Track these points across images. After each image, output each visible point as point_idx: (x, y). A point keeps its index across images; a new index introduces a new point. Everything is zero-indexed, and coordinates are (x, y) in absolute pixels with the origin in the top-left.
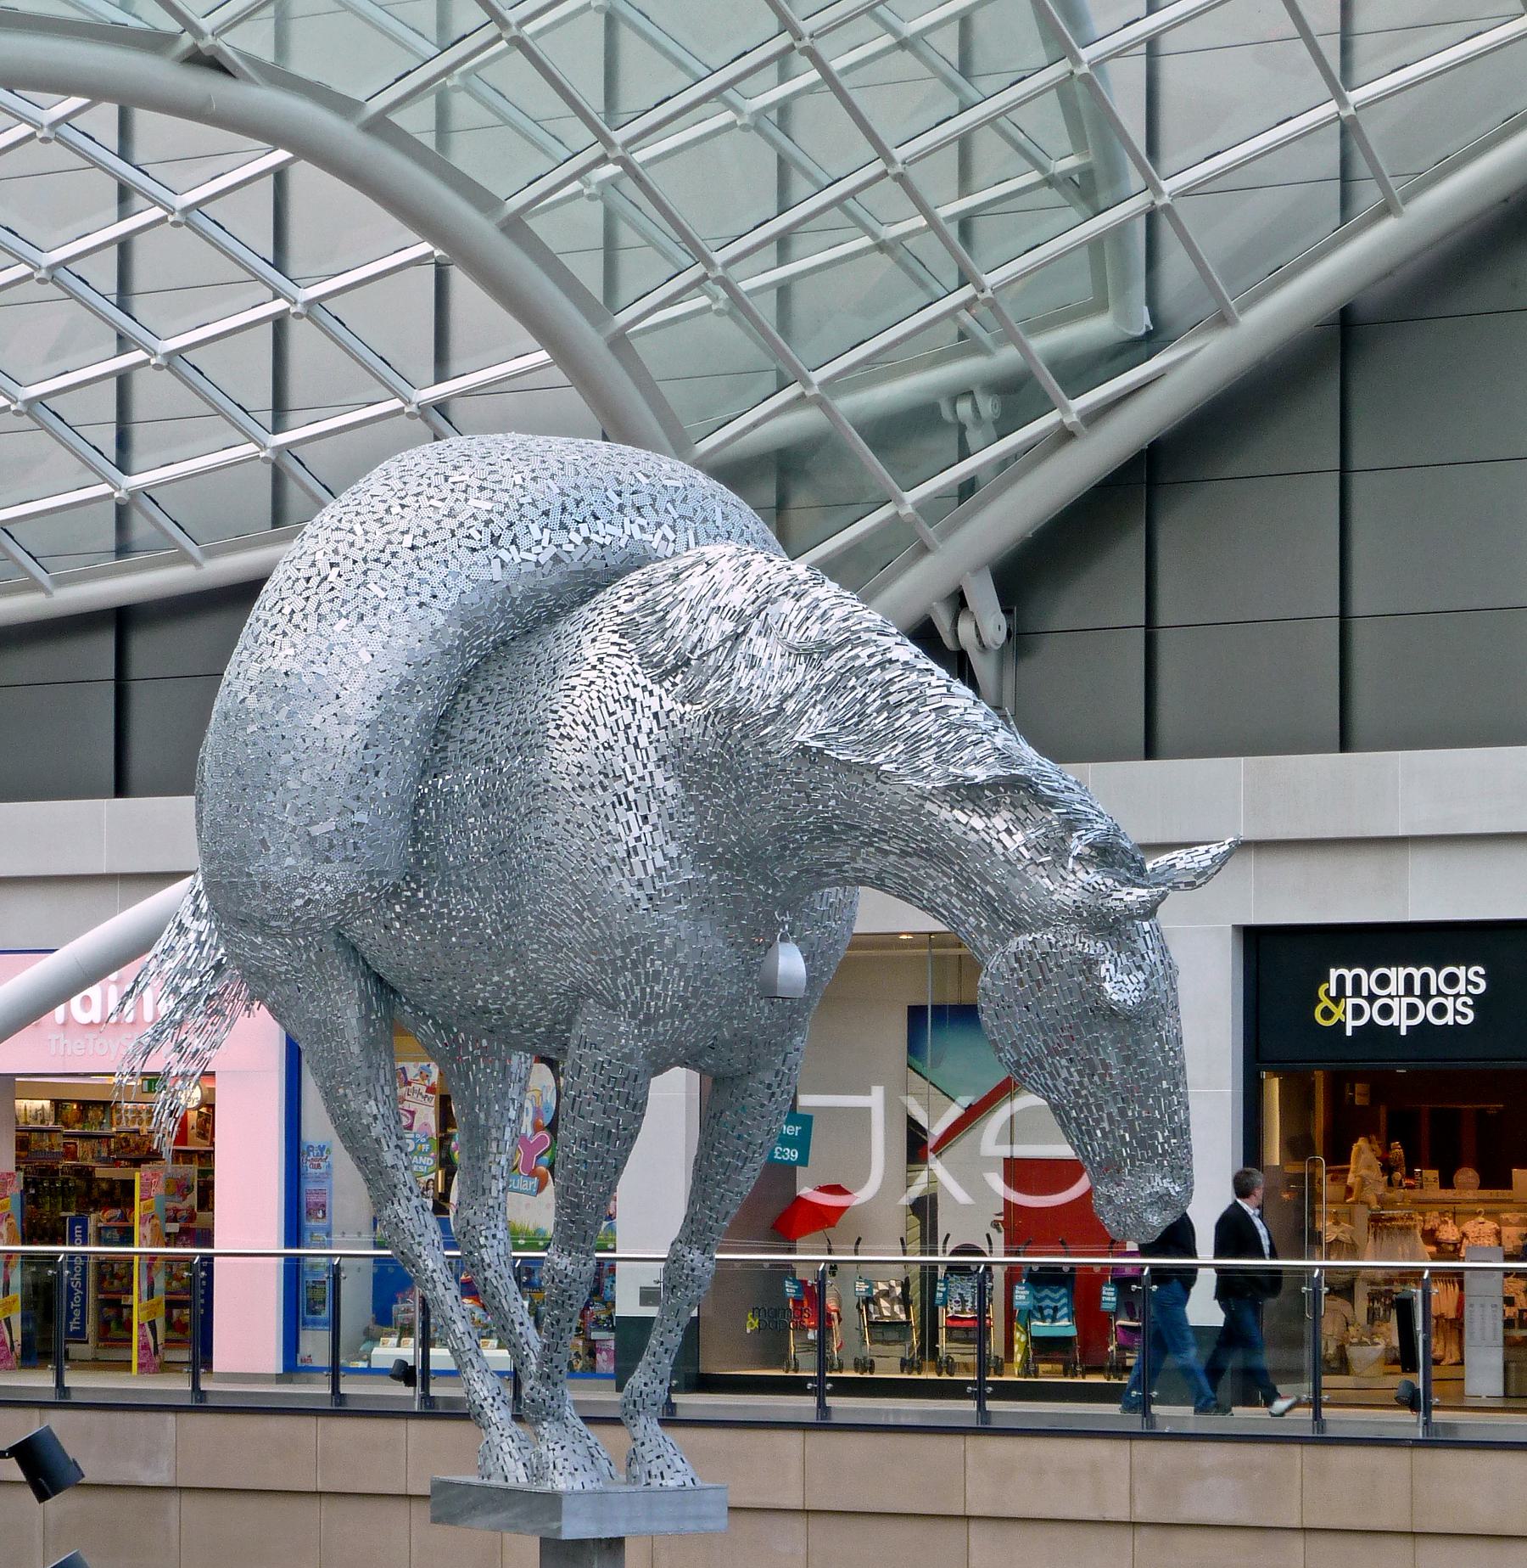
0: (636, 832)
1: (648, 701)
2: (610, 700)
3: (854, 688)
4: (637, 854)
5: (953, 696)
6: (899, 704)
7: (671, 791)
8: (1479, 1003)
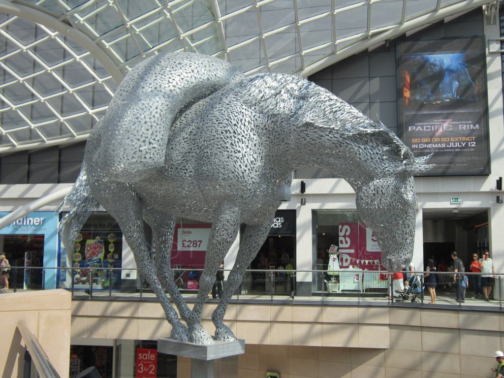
0: (245, 150)
1: (247, 113)
2: (235, 113)
3: (320, 107)
4: (245, 156)
5: (352, 109)
6: (336, 111)
7: (255, 139)
8: (282, 224)
